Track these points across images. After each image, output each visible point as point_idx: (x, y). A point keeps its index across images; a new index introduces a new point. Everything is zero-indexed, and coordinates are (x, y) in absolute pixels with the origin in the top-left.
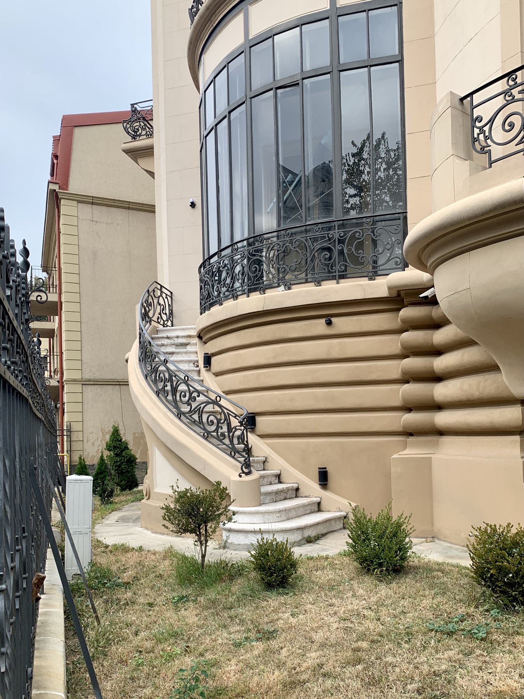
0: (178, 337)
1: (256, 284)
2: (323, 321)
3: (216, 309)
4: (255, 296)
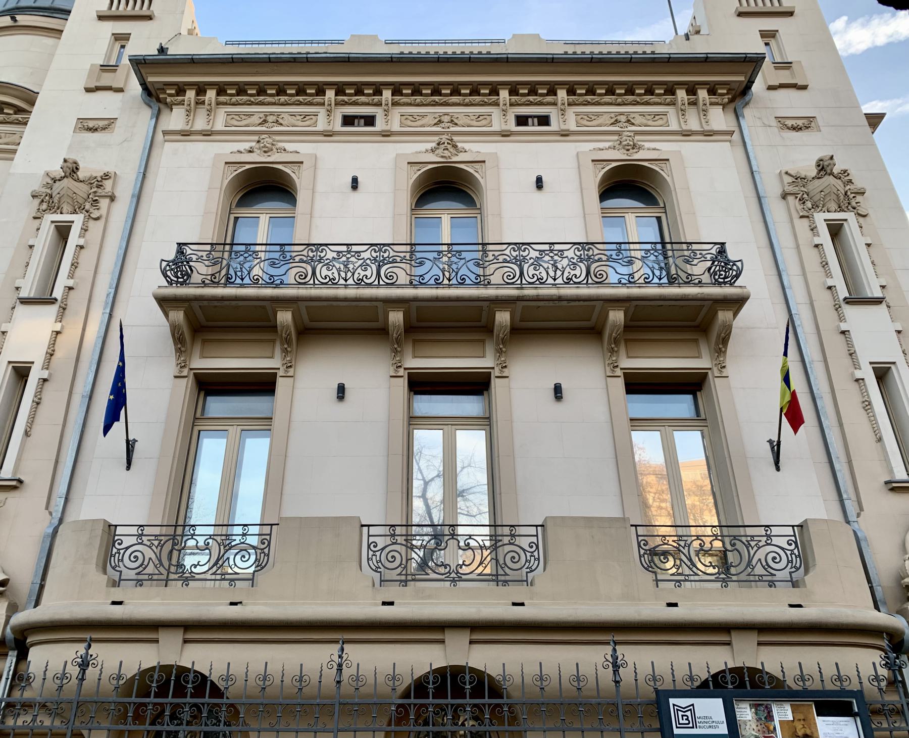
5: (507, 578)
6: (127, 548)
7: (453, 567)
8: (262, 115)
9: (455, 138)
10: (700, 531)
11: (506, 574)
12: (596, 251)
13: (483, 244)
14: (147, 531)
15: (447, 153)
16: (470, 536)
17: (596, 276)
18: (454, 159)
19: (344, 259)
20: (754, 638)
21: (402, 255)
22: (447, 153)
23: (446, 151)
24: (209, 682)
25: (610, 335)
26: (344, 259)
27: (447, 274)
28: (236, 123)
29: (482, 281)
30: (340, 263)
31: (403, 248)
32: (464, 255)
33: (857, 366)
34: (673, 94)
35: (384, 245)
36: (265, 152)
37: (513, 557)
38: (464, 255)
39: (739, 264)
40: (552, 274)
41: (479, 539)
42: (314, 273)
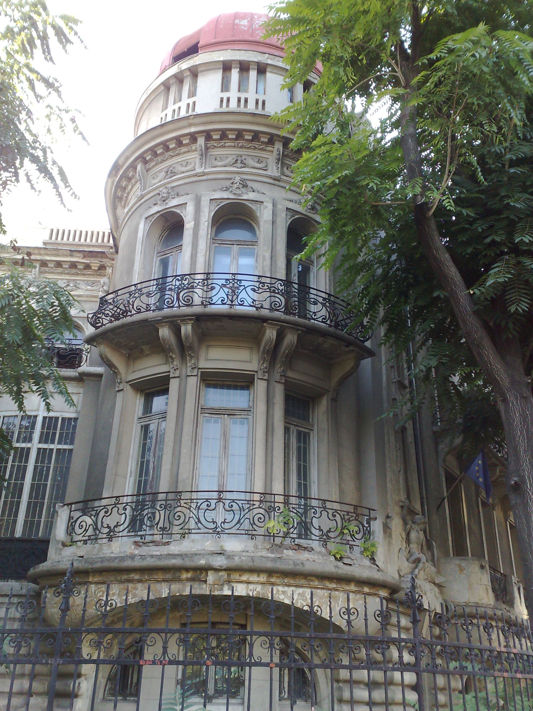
5: (254, 533)
7: (325, 531)
8: (234, 157)
10: (206, 495)
11: (255, 530)
13: (208, 274)
14: (328, 505)
15: (238, 192)
16: (234, 500)
18: (245, 197)
19: (231, 285)
22: (238, 192)
23: (238, 190)
24: (293, 610)
25: (265, 348)
26: (231, 285)
27: (230, 297)
28: (184, 169)
29: (190, 305)
30: (228, 288)
32: (243, 283)
35: (185, 275)
36: (164, 201)
37: (261, 518)
38: (243, 283)
40: (230, 297)
41: (240, 503)
42: (178, 299)
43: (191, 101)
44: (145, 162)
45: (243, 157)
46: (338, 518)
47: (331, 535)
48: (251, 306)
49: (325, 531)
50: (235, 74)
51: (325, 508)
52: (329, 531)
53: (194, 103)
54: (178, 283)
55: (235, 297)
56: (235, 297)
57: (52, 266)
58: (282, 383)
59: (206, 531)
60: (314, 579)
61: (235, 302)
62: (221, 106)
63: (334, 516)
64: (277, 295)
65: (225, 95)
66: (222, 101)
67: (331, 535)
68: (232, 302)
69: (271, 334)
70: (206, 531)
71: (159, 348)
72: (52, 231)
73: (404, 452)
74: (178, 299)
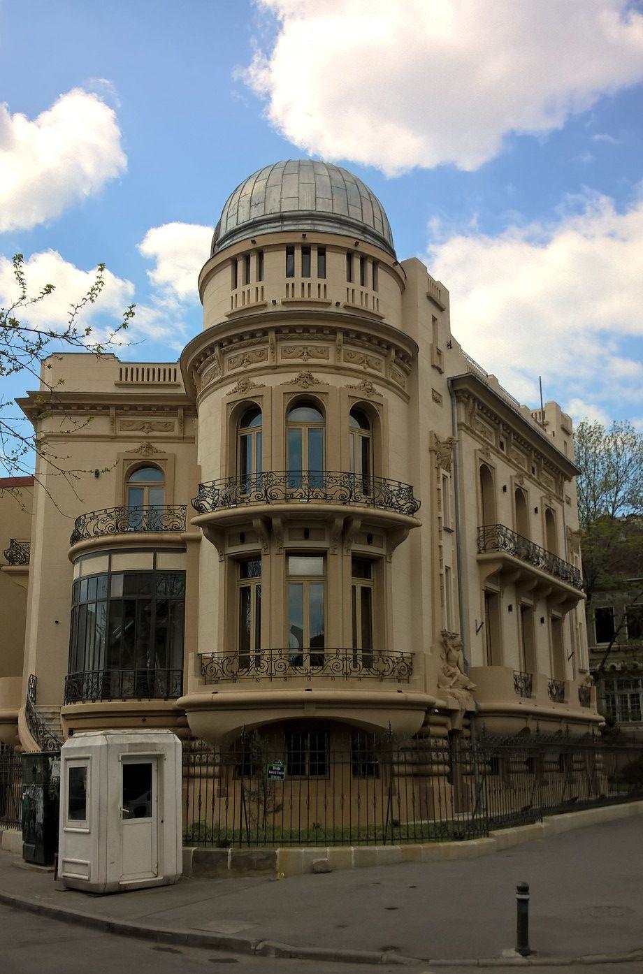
0: (46, 713)
1: (107, 696)
2: (141, 719)
3: (79, 704)
4: (106, 702)
6: (207, 666)
7: (381, 671)
9: (150, 440)
12: (275, 477)
17: (271, 496)
20: (315, 706)
21: (280, 478)
27: (307, 494)
31: (339, 475)
33: (441, 567)
34: (335, 334)
39: (418, 503)
40: (307, 494)
42: (266, 495)
43: (259, 284)
44: (221, 346)
45: (309, 348)
46: (390, 662)
47: (385, 673)
48: (323, 499)
49: (381, 671)
50: (298, 254)
51: (381, 656)
52: (384, 671)
53: (262, 287)
54: (264, 479)
55: (311, 493)
56: (311, 493)
57: (75, 408)
58: (433, 737)
59: (302, 675)
60: (388, 786)
61: (311, 497)
62: (287, 296)
63: (388, 661)
64: (346, 490)
65: (290, 281)
66: (287, 285)
67: (385, 673)
68: (308, 496)
69: (340, 522)
70: (302, 675)
71: (255, 535)
72: (121, 370)
73: (58, 436)
74: (266, 495)
